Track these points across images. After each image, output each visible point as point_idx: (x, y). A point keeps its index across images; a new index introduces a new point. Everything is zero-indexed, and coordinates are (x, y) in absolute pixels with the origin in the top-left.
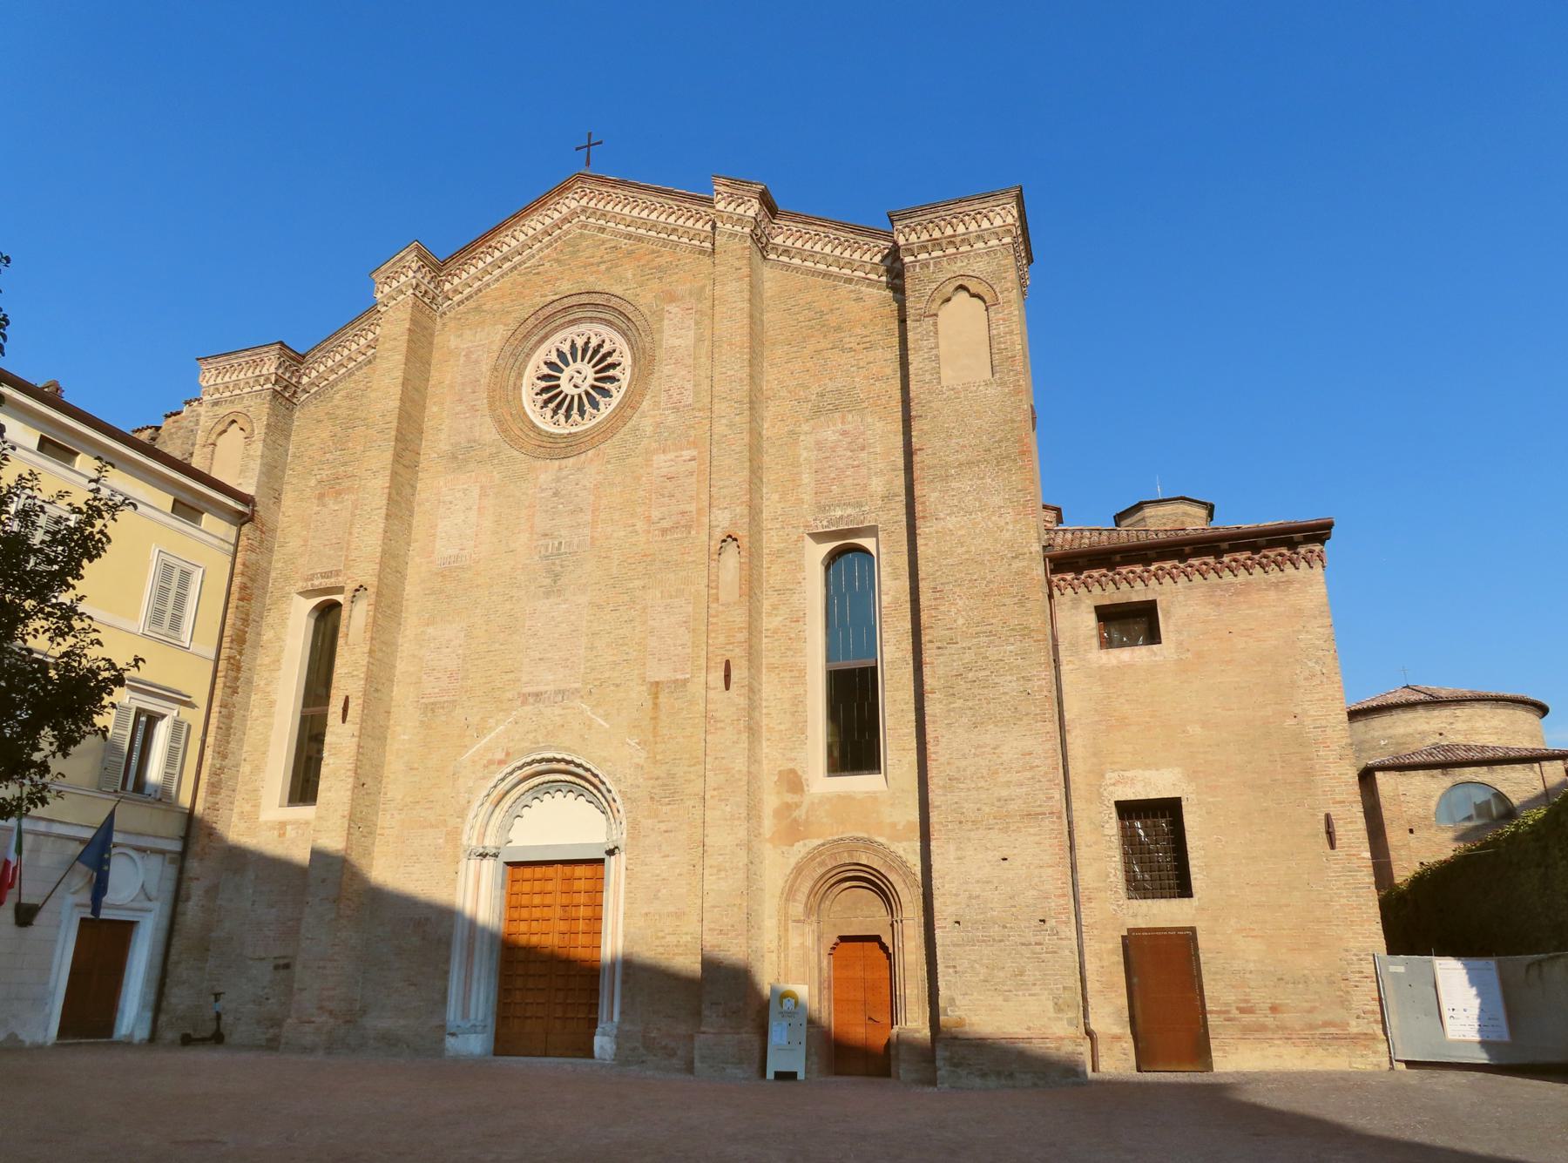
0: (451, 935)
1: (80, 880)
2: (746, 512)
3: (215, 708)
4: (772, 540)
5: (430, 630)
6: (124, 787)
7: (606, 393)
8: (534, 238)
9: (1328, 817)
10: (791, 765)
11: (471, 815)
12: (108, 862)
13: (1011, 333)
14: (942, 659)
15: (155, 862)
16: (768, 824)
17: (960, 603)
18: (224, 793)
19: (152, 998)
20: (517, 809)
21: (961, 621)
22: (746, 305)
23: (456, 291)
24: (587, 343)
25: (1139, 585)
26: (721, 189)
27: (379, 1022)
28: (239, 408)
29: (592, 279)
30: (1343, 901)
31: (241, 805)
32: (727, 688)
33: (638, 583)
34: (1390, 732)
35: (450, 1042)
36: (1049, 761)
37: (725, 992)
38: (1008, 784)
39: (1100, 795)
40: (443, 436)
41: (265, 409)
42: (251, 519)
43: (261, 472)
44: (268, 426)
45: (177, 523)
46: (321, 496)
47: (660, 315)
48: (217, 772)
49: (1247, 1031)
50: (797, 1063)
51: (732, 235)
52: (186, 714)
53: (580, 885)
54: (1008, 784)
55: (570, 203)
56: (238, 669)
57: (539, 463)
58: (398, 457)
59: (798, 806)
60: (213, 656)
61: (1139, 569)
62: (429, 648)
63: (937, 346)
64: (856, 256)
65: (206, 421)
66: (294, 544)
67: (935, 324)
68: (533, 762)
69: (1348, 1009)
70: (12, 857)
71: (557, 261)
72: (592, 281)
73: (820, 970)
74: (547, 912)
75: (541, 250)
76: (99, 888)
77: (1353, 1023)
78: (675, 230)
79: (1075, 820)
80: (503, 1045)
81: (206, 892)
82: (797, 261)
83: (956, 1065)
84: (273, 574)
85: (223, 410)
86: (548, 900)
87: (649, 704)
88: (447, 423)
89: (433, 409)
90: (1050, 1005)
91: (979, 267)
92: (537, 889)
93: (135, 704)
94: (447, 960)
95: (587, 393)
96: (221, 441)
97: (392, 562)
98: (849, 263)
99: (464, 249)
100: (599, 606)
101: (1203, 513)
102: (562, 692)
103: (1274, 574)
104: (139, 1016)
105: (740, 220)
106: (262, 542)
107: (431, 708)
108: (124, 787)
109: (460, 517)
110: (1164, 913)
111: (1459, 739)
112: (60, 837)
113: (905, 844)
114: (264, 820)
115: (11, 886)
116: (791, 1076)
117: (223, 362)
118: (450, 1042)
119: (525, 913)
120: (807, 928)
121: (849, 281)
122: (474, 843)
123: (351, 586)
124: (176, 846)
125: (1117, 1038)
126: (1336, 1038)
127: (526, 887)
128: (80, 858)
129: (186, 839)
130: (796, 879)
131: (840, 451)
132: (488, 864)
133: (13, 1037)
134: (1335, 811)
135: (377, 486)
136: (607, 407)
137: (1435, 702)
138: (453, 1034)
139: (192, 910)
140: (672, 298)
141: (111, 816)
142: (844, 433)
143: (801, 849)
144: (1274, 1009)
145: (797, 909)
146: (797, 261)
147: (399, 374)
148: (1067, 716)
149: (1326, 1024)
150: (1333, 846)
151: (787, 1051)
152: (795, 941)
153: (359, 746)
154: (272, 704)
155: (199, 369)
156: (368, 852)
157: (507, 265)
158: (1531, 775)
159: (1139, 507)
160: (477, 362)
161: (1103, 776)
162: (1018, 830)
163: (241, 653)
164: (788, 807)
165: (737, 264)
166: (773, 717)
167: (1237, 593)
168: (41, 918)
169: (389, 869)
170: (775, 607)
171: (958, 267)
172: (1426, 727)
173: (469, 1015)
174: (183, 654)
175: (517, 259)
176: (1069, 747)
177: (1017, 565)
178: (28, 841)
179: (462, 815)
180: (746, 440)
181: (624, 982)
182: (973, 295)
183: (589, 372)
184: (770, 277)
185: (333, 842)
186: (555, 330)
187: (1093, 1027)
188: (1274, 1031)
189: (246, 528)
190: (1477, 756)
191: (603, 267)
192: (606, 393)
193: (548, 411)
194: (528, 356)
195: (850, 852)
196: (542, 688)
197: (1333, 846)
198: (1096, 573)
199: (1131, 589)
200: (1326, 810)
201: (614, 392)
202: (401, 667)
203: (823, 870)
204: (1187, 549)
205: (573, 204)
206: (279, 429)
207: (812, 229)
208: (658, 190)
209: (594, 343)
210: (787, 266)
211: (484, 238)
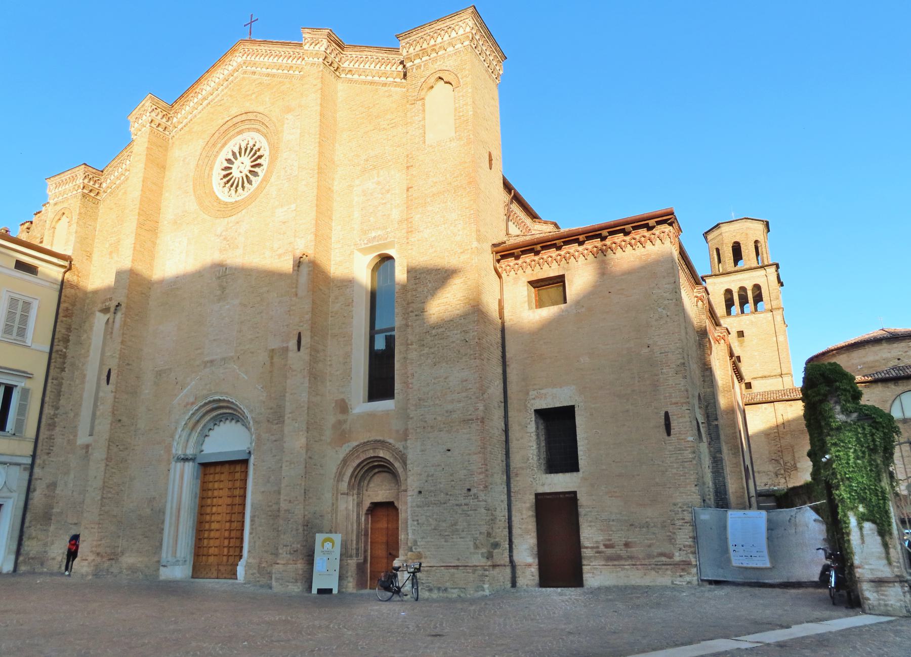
2: (313, 238)
7: (255, 174)
9: (667, 414)
10: (342, 396)
11: (177, 437)
13: (466, 104)
14: (418, 322)
17: (430, 285)
19: (14, 547)
22: (319, 108)
23: (179, 123)
24: (240, 148)
28: (65, 205)
30: (674, 471)
32: (299, 349)
34: (865, 360)
36: (477, 385)
38: (452, 401)
39: (526, 406)
41: (78, 204)
49: (609, 559)
51: (313, 64)
53: (238, 476)
54: (452, 401)
55: (237, 59)
59: (345, 421)
60: (48, 350)
63: (424, 119)
65: (51, 215)
67: (424, 105)
71: (231, 96)
72: (249, 106)
75: (223, 90)
77: (677, 554)
78: (291, 67)
79: (510, 423)
82: (356, 77)
85: (58, 207)
90: (471, 544)
91: (450, 64)
92: (216, 479)
94: (163, 522)
95: (247, 176)
100: (245, 306)
101: (760, 227)
105: (317, 55)
110: (560, 483)
116: (329, 591)
120: (350, 498)
121: (385, 85)
122: (180, 452)
125: (530, 565)
130: (343, 467)
134: (672, 410)
138: (164, 566)
139: (38, 497)
140: (289, 110)
142: (379, 183)
143: (346, 449)
144: (627, 545)
145: (344, 486)
146: (356, 77)
147: (141, 175)
148: (508, 355)
150: (669, 434)
152: (342, 506)
153: (115, 398)
154: (84, 376)
155: (46, 185)
157: (205, 102)
159: (717, 226)
161: (528, 394)
163: (66, 348)
171: (437, 66)
172: (889, 355)
175: (211, 97)
176: (508, 375)
179: (172, 436)
180: (315, 194)
182: (446, 83)
184: (341, 89)
186: (230, 139)
187: (516, 558)
188: (626, 559)
191: (254, 96)
192: (255, 174)
193: (226, 189)
194: (216, 156)
196: (215, 357)
197: (669, 434)
200: (666, 409)
201: (260, 173)
205: (239, 60)
208: (283, 44)
209: (251, 145)
210: (350, 81)
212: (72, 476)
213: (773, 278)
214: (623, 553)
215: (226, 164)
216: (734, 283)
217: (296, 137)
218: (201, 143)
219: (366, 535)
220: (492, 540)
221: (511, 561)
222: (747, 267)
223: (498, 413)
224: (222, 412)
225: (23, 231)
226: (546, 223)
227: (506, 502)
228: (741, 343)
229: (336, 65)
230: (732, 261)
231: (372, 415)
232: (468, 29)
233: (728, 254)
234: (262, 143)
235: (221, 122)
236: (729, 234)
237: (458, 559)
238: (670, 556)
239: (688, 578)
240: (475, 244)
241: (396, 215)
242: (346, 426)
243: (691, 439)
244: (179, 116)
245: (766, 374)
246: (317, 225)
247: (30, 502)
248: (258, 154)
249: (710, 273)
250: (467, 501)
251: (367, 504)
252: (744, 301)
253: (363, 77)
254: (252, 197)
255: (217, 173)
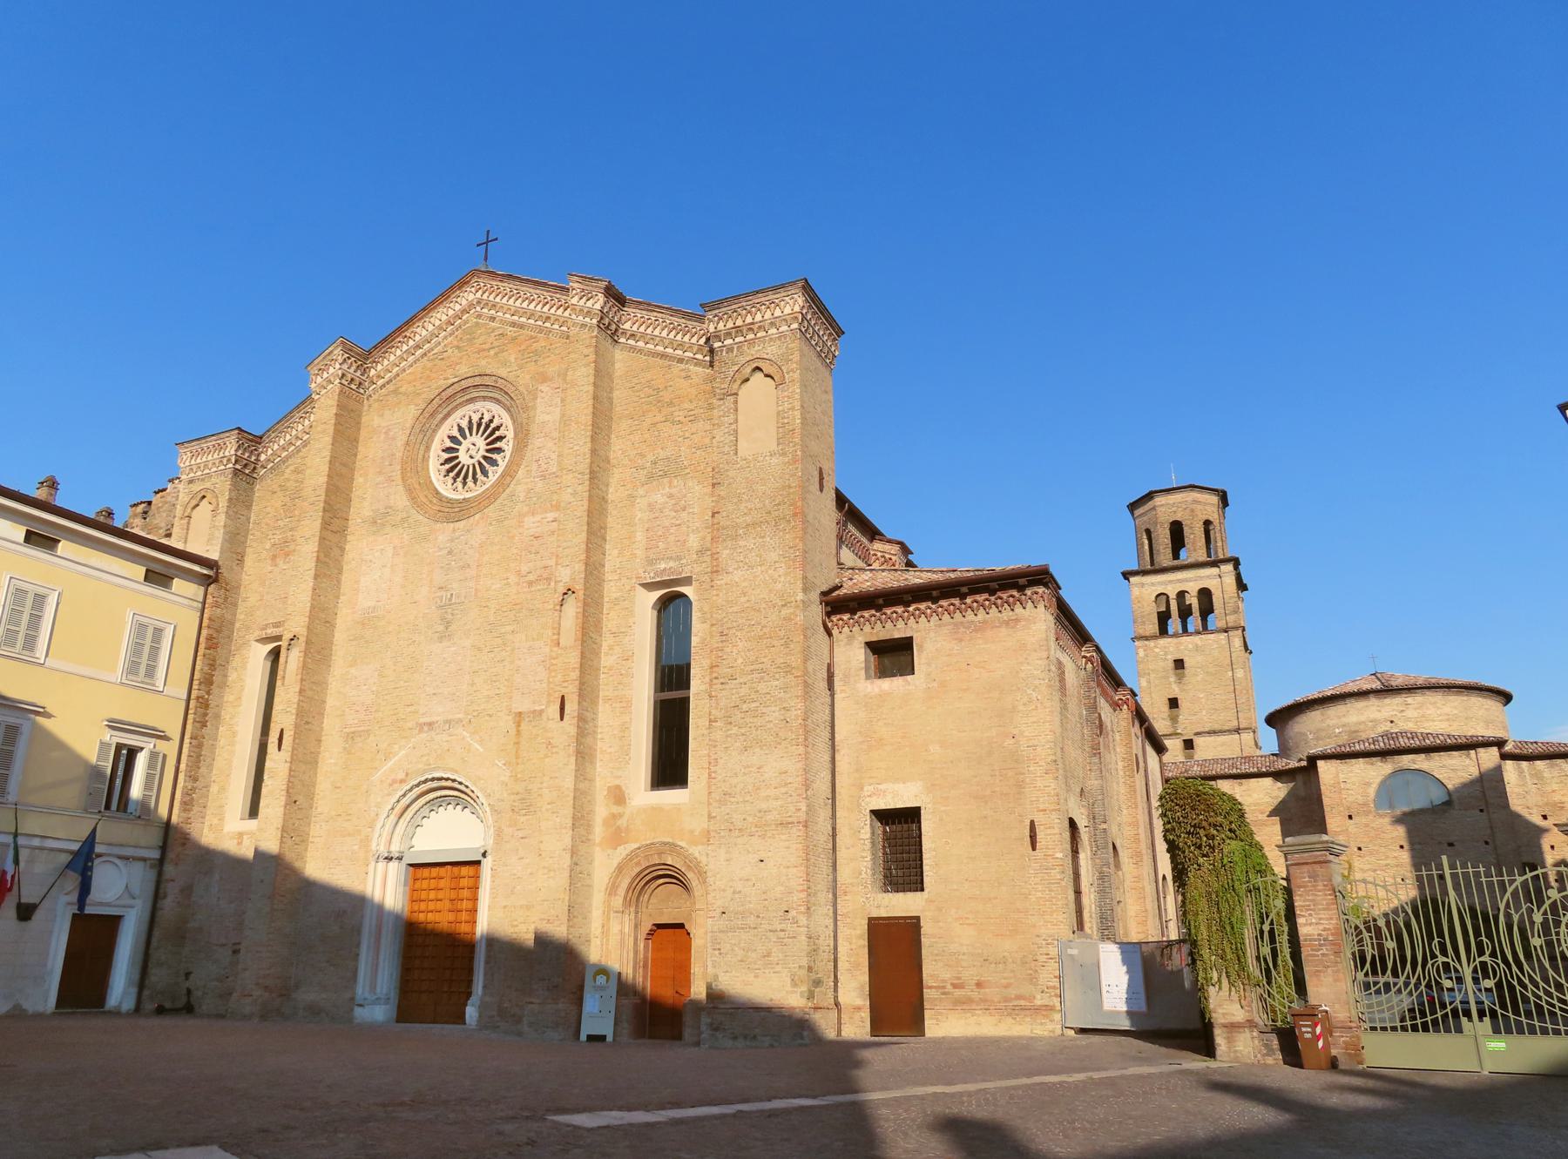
0: (361, 924)
1: (72, 882)
3: (187, 740)
4: (611, 590)
5: (353, 670)
6: (108, 807)
7: (494, 463)
8: (440, 328)
9: (1032, 823)
10: (617, 782)
11: (379, 825)
12: (91, 869)
15: (138, 868)
16: (598, 831)
18: (196, 809)
19: (136, 977)
20: (418, 820)
21: (740, 661)
22: (591, 388)
23: (379, 377)
24: (470, 422)
25: (901, 624)
26: (576, 285)
27: (306, 996)
28: (208, 485)
29: (483, 362)
31: (210, 819)
33: (509, 628)
34: (1345, 720)
35: (358, 1011)
37: (552, 966)
39: (859, 805)
40: (366, 504)
42: (216, 580)
43: (225, 540)
44: (230, 500)
45: (149, 589)
46: (274, 557)
47: (534, 395)
48: (188, 793)
49: (959, 1002)
50: (606, 1028)
51: (583, 326)
52: (162, 746)
53: (464, 882)
55: (468, 296)
56: (207, 706)
57: (439, 525)
58: (326, 525)
59: (621, 815)
61: (900, 609)
62: (350, 685)
64: (686, 339)
65: (183, 498)
66: (253, 599)
67: (736, 402)
68: (425, 781)
69: (1036, 985)
70: (10, 868)
72: (487, 365)
73: (636, 952)
74: (439, 905)
76: (85, 889)
78: (548, 318)
80: (405, 1013)
81: (182, 891)
82: (641, 344)
83: (716, 1029)
84: (237, 625)
85: (196, 487)
86: (441, 895)
87: (513, 732)
88: (373, 490)
89: (359, 480)
91: (772, 350)
93: (115, 740)
94: (358, 945)
96: (195, 514)
97: (321, 616)
98: (681, 345)
99: (385, 340)
100: (479, 649)
101: (1214, 499)
102: (448, 722)
103: (1007, 613)
104: (125, 993)
106: (226, 599)
107: (351, 737)
108: (108, 807)
109: (377, 570)
110: (900, 904)
111: (1410, 726)
112: (52, 850)
113: (700, 847)
114: (228, 828)
115: (10, 890)
116: (602, 1038)
117: (195, 446)
118: (358, 1011)
119: (423, 906)
121: (681, 361)
123: (287, 636)
124: (156, 854)
125: (859, 1009)
126: (1023, 1009)
127: (425, 884)
128: (69, 866)
129: (164, 848)
131: (667, 512)
132: (393, 865)
133: (17, 1007)
134: (1039, 819)
135: (307, 551)
136: (494, 473)
137: (1387, 691)
139: (168, 904)
140: (544, 378)
141: (94, 831)
142: (671, 496)
143: (622, 851)
145: (618, 901)
146: (641, 344)
147: (327, 453)
149: (1019, 997)
150: (1034, 848)
151: (598, 1015)
152: (615, 928)
154: (234, 734)
156: (301, 857)
158: (1468, 761)
159: (1149, 496)
160: (394, 439)
162: (773, 837)
163: (208, 693)
164: (614, 817)
165: (586, 351)
166: (605, 742)
167: (976, 631)
168: (38, 916)
169: (318, 867)
170: (611, 648)
171: (754, 351)
172: (1377, 715)
173: (375, 988)
174: (157, 696)
177: (785, 612)
178: (23, 854)
179: (372, 827)
181: (487, 962)
183: (481, 443)
184: (620, 359)
185: (271, 845)
186: (456, 408)
187: (840, 999)
189: (212, 588)
190: (1416, 743)
192: (494, 463)
193: (449, 479)
194: (435, 431)
195: (660, 854)
196: (434, 719)
197: (1034, 848)
198: (866, 614)
199: (892, 626)
202: (331, 702)
203: (638, 869)
204: (935, 593)
205: (471, 297)
206: (241, 501)
207: (653, 315)
209: (487, 418)
211: (400, 330)
212: (217, 876)
213: (1230, 580)
214: (975, 995)
215: (449, 444)
216: (1170, 584)
217: (556, 416)
218: (413, 411)
219: (645, 966)
220: (813, 976)
221: (837, 1004)
222: (1191, 560)
223: (824, 814)
224: (445, 791)
225: (135, 515)
226: (889, 541)
227: (831, 927)
228: (1180, 678)
229: (613, 327)
230: (1169, 551)
231: (657, 809)
232: (797, 308)
233: (1163, 538)
234: (502, 417)
235: (443, 383)
236: (1167, 508)
237: (1545, 817)
238: (1032, 998)
239: (1050, 1027)
240: (800, 596)
241: (694, 542)
242: (622, 822)
243: (1060, 855)
244: (379, 367)
245: (1217, 727)
246: (588, 550)
247: (159, 913)
248: (497, 434)
249: (1135, 567)
250: (783, 926)
251: (647, 927)
252: (1185, 613)
253: (650, 346)
254: (490, 497)
255: (436, 456)
